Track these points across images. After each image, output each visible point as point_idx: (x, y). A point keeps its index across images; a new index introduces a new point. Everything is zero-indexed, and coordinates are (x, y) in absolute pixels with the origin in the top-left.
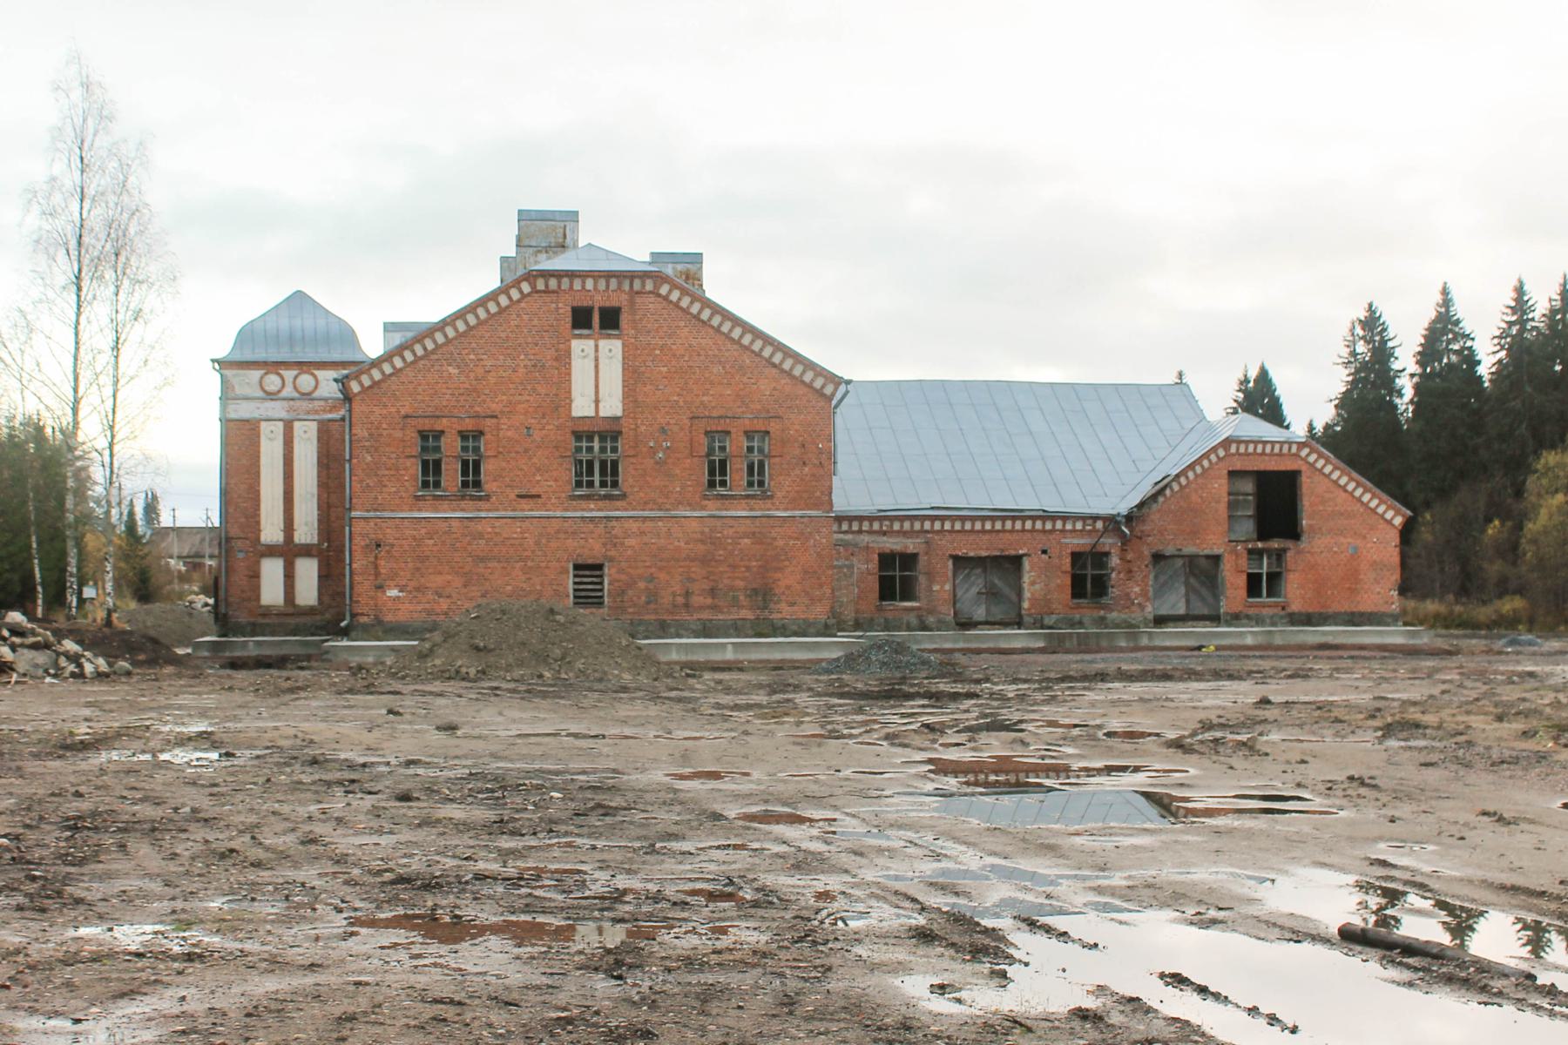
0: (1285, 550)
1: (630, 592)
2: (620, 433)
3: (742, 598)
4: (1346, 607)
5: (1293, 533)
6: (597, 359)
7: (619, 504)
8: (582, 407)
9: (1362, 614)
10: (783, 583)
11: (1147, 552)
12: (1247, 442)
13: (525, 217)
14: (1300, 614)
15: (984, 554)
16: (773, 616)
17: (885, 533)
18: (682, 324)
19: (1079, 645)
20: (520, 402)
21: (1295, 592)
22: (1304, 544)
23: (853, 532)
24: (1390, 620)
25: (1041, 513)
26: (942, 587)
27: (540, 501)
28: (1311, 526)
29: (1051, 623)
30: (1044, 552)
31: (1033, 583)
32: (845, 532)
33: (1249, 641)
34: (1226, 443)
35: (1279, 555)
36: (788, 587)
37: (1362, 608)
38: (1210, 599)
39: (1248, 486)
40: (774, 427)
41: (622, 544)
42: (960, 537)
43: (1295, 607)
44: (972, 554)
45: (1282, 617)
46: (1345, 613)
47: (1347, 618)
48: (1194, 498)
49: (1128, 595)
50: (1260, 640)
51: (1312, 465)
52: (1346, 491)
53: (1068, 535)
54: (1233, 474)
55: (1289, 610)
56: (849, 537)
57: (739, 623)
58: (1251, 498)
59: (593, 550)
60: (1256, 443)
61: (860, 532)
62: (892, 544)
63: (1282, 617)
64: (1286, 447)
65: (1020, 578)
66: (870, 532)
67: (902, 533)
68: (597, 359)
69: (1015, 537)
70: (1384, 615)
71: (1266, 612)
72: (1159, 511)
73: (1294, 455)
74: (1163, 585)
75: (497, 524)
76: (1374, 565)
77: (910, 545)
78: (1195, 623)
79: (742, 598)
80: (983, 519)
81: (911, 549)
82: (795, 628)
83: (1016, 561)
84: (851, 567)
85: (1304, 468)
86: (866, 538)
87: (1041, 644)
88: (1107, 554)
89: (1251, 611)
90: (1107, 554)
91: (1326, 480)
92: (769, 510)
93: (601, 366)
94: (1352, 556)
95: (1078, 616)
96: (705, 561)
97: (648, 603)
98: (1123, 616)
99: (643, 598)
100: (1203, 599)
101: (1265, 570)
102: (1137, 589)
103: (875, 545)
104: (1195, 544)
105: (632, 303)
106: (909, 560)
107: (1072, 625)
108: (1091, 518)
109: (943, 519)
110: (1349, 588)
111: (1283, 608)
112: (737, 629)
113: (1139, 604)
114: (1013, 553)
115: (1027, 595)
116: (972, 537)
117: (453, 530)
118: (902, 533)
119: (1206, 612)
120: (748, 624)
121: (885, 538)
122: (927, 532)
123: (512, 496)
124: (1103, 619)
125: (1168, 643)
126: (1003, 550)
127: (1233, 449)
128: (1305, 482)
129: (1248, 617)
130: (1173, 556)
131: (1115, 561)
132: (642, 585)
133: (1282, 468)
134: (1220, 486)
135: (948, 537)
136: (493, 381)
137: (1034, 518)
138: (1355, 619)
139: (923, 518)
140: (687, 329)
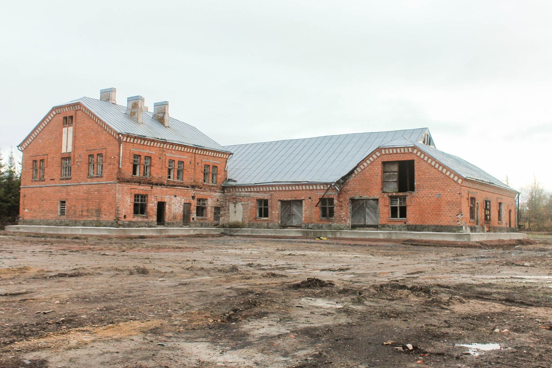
0: (405, 196)
1: (71, 211)
2: (70, 157)
3: (94, 213)
4: (436, 223)
5: (412, 189)
6: (67, 134)
7: (70, 181)
8: (64, 151)
9: (442, 226)
10: (103, 207)
11: (348, 197)
12: (389, 149)
13: (101, 90)
14: (412, 225)
15: (289, 199)
16: (101, 219)
17: (258, 192)
18: (86, 119)
19: (314, 235)
20: (52, 150)
21: (411, 217)
22: (414, 194)
23: (249, 192)
24: (455, 229)
25: (307, 183)
26: (275, 212)
27: (54, 181)
28: (418, 185)
29: (311, 227)
30: (310, 198)
31: (306, 211)
32: (246, 192)
33: (381, 237)
34: (379, 149)
35: (404, 199)
36: (105, 209)
37: (442, 223)
38: (374, 218)
39: (395, 168)
40: (104, 152)
41: (70, 194)
42: (283, 193)
43: (410, 222)
44: (285, 199)
45: (404, 227)
46: (434, 226)
47: (433, 228)
48: (367, 174)
49: (340, 216)
50: (386, 237)
51: (419, 157)
52: (435, 168)
53: (318, 191)
54: (384, 163)
55: (407, 224)
56: (248, 193)
57: (92, 221)
58: (396, 173)
59: (64, 197)
60: (393, 148)
61: (251, 192)
62: (260, 196)
63: (404, 227)
64: (406, 149)
65: (302, 208)
66: (254, 192)
67: (263, 192)
68: (67, 134)
69: (301, 192)
70: (452, 226)
71: (399, 224)
72: (353, 180)
73: (411, 153)
74: (355, 212)
75: (46, 189)
76: (448, 203)
77: (266, 196)
78: (360, 229)
79: (94, 213)
80: (289, 185)
81: (266, 198)
82: (104, 224)
83: (301, 201)
84: (248, 204)
85: (415, 159)
86: (252, 194)
87: (300, 235)
88: (333, 199)
89: (390, 224)
90: (333, 199)
91: (426, 164)
92: (102, 181)
93: (68, 135)
94: (438, 198)
95: (321, 224)
96: (87, 200)
97: (74, 214)
98: (338, 225)
99: (73, 213)
100: (371, 218)
101: (398, 206)
102: (344, 213)
103: (255, 196)
104: (367, 194)
105: (76, 114)
106: (266, 202)
107: (319, 228)
108: (325, 184)
109: (275, 186)
110: (436, 214)
111: (405, 223)
112: (91, 224)
113: (345, 220)
114: (299, 199)
115: (304, 215)
116: (286, 192)
117: (38, 191)
118: (263, 192)
119: (372, 224)
120: (94, 222)
121: (258, 194)
122: (271, 191)
123: (49, 179)
124: (330, 225)
125: (347, 237)
126: (296, 198)
127: (415, 151)
128: (417, 166)
129: (388, 226)
130: (358, 200)
131: (335, 201)
132: (73, 208)
133: (405, 159)
134: (378, 169)
135: (278, 193)
136: (48, 143)
137: (305, 185)
138: (439, 229)
139: (269, 186)
140: (87, 121)
